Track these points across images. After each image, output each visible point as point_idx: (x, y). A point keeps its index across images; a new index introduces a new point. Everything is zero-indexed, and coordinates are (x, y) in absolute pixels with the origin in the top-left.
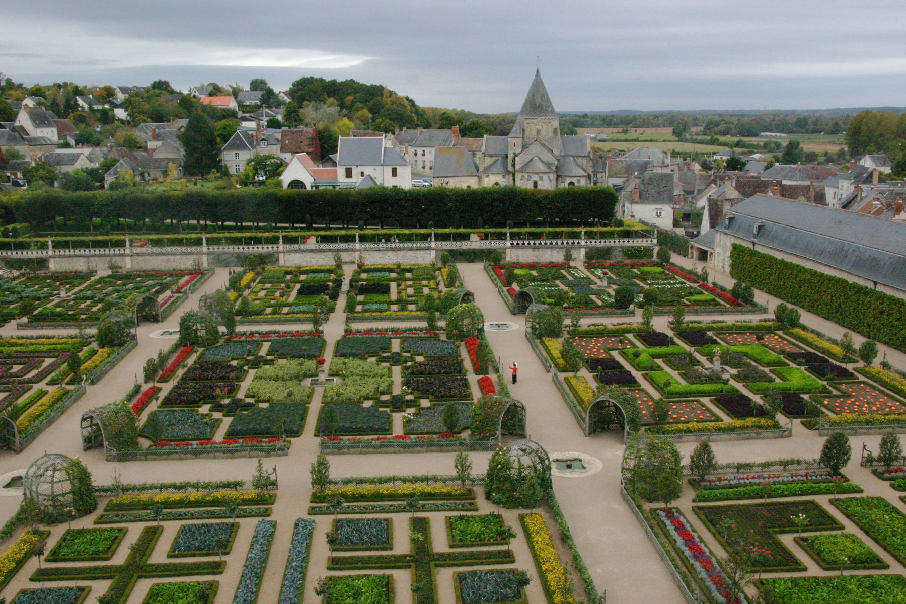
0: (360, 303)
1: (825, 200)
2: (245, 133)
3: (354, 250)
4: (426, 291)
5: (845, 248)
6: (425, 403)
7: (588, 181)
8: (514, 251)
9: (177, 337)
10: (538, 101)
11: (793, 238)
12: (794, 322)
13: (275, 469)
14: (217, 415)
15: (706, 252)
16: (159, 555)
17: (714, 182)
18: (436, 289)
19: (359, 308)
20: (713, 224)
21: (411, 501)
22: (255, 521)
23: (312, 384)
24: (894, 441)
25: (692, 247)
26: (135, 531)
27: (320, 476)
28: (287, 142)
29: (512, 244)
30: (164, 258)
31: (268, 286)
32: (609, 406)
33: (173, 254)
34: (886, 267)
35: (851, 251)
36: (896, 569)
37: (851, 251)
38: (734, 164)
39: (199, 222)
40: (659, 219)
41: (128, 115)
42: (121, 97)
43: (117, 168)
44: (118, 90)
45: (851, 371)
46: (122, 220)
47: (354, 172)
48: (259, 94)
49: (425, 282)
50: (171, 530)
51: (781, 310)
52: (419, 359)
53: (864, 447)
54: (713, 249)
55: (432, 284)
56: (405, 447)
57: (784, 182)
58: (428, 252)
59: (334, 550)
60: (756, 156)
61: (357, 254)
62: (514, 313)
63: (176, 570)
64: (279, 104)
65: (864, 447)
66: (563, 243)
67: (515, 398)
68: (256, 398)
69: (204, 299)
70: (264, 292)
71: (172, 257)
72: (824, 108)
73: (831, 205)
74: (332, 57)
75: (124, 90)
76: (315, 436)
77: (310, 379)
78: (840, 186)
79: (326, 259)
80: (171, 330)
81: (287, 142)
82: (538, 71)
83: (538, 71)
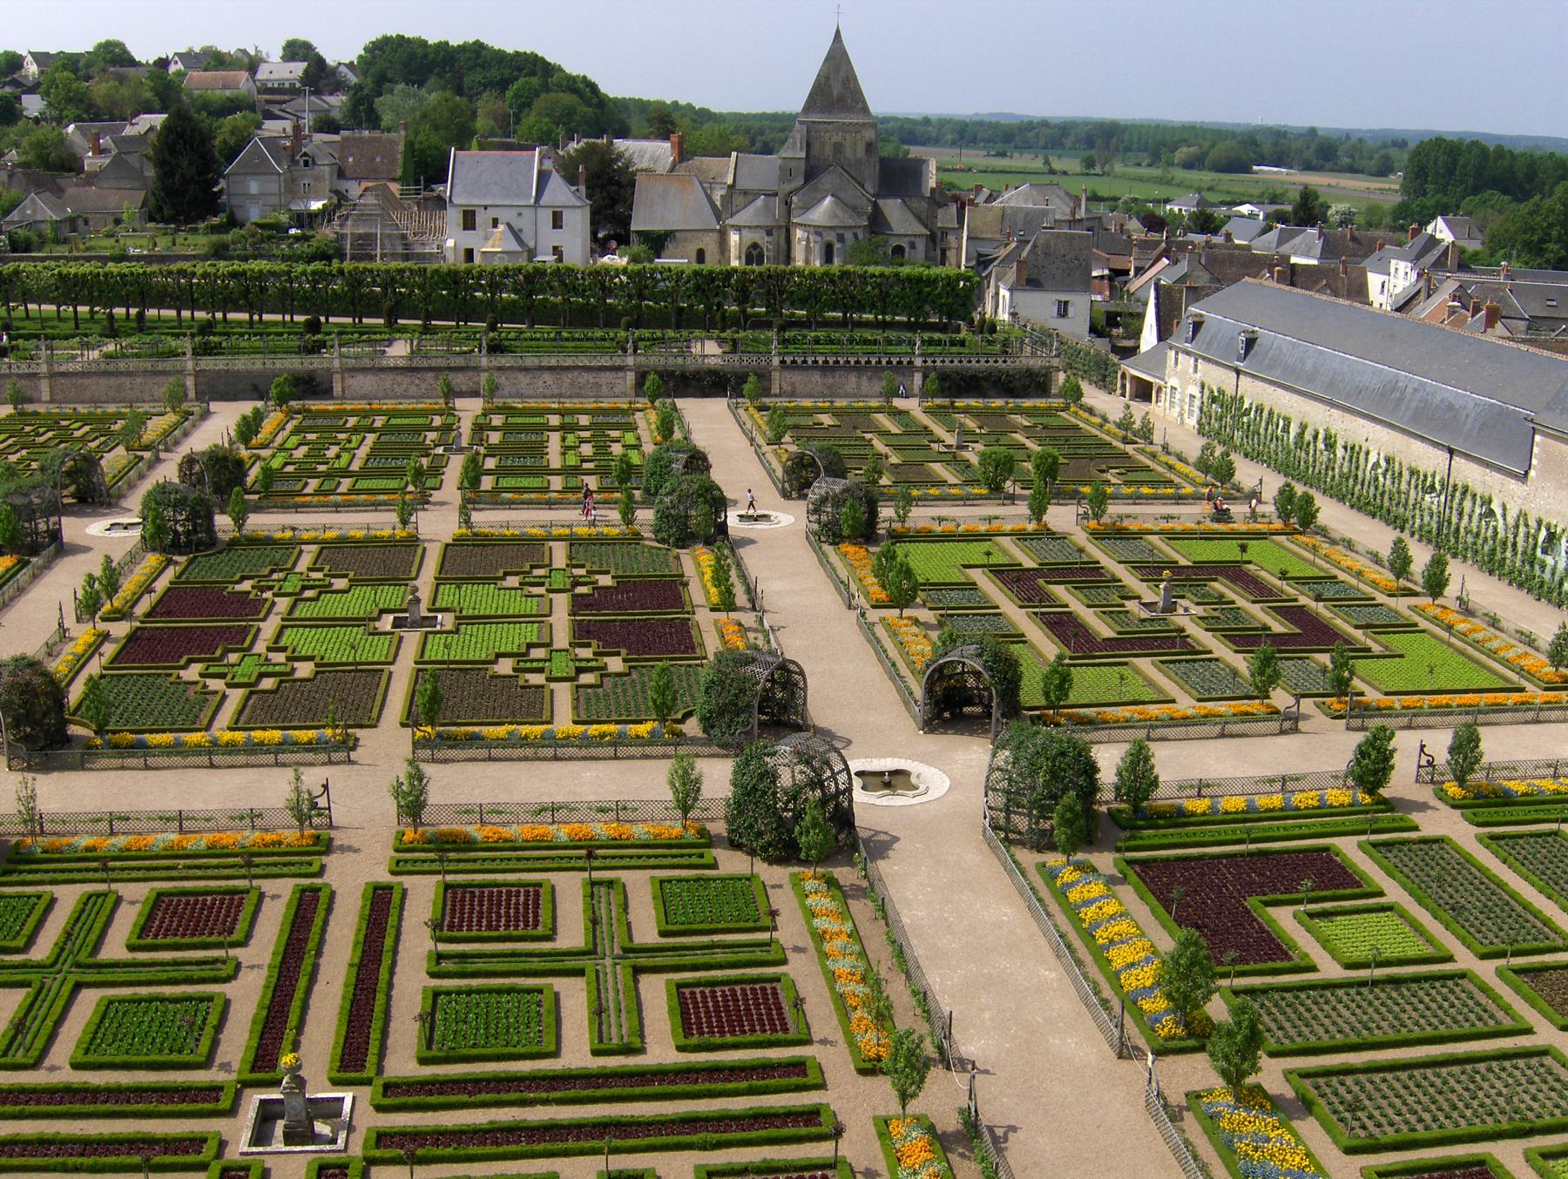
0: (489, 472)
1: (1367, 296)
2: (270, 142)
3: (477, 369)
4: (617, 449)
5: (1400, 384)
6: (615, 664)
7: (931, 245)
8: (787, 374)
9: (136, 533)
10: (836, 89)
11: (1309, 365)
12: (1307, 516)
13: (326, 787)
14: (215, 684)
15: (1149, 385)
16: (115, 948)
17: (1166, 253)
18: (637, 447)
19: (487, 483)
20: (1163, 334)
21: (588, 852)
22: (106, 954)
23: (394, 626)
24: (1474, 740)
25: (1124, 376)
26: (68, 897)
27: (413, 805)
28: (351, 160)
29: (783, 362)
30: (113, 381)
31: (312, 437)
32: (963, 672)
33: (129, 374)
34: (1470, 420)
35: (1410, 390)
36: (1546, 1034)
37: (1410, 390)
38: (1205, 223)
39: (179, 314)
40: (1063, 321)
41: (50, 105)
42: (32, 69)
43: (25, 209)
44: (29, 58)
45: (1407, 613)
46: (32, 307)
47: (479, 219)
48: (299, 68)
49: (615, 434)
50: (136, 895)
51: (1286, 496)
52: (605, 581)
53: (1423, 747)
54: (1163, 379)
55: (630, 438)
56: (584, 748)
57: (1294, 260)
58: (621, 374)
59: (439, 940)
60: (1245, 209)
61: (484, 377)
62: (786, 495)
63: (455, 842)
64: (338, 86)
65: (1423, 747)
66: (880, 362)
67: (788, 656)
68: (289, 653)
69: (190, 461)
70: (304, 450)
71: (126, 381)
72: (1364, 128)
73: (1376, 305)
74: (1450, 1051)
75: (40, 58)
76: (403, 725)
77: (391, 617)
78: (1392, 270)
79: (424, 386)
80: (126, 520)
81: (351, 160)
82: (838, 33)
83: (838, 33)
